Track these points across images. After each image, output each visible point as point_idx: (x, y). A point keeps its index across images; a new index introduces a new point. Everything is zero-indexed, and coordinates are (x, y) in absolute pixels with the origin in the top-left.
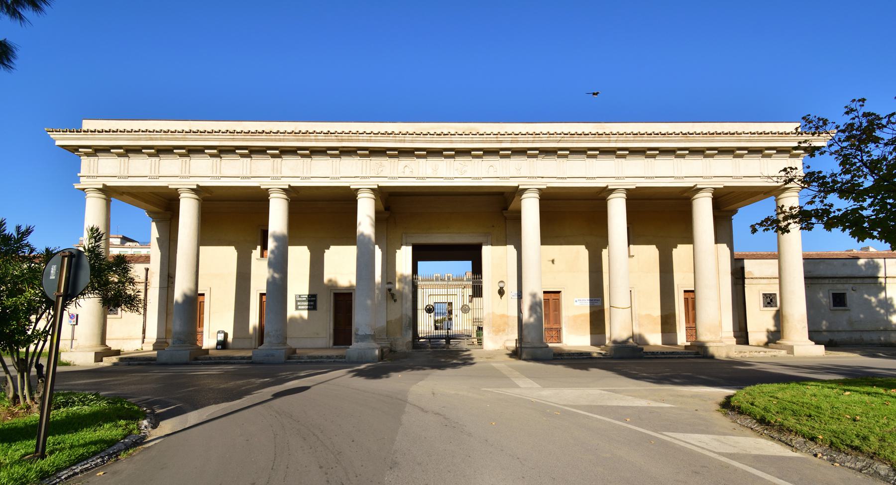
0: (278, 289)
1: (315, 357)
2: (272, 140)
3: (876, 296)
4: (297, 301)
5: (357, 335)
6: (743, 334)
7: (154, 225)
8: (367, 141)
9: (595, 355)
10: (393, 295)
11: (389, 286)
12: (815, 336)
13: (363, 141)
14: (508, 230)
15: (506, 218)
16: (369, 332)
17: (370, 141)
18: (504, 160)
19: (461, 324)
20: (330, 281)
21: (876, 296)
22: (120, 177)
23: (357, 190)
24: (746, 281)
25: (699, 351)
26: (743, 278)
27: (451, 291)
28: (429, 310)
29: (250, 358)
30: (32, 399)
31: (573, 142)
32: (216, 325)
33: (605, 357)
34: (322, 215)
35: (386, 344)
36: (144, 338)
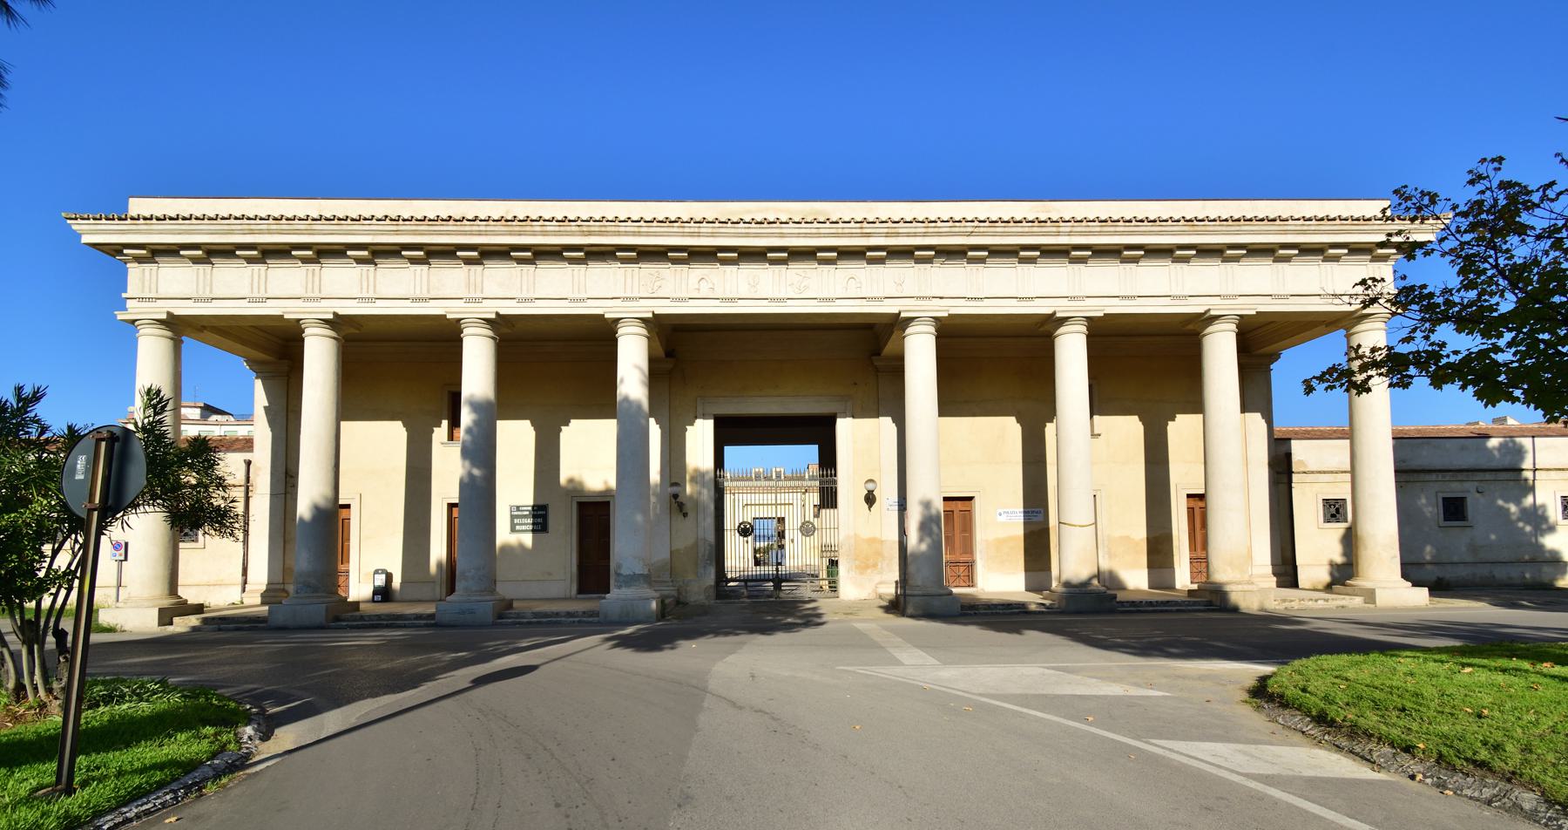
0: (479, 494)
1: (546, 615)
2: (464, 233)
3: (1518, 502)
4: (513, 517)
5: (618, 575)
6: (1289, 568)
7: (259, 384)
8: (634, 234)
9: (1033, 607)
10: (681, 506)
11: (675, 489)
12: (1412, 571)
13: (626, 234)
14: (884, 394)
15: (877, 370)
16: (639, 569)
17: (639, 234)
18: (874, 268)
19: (799, 555)
20: (571, 481)
21: (1518, 502)
22: (197, 300)
23: (617, 320)
24: (1295, 477)
25: (1212, 599)
26: (1289, 472)
27: (782, 498)
28: (745, 531)
29: (431, 616)
30: (49, 691)
31: (994, 235)
32: (372, 559)
33: (1049, 611)
34: (556, 365)
35: (669, 590)
36: (245, 582)
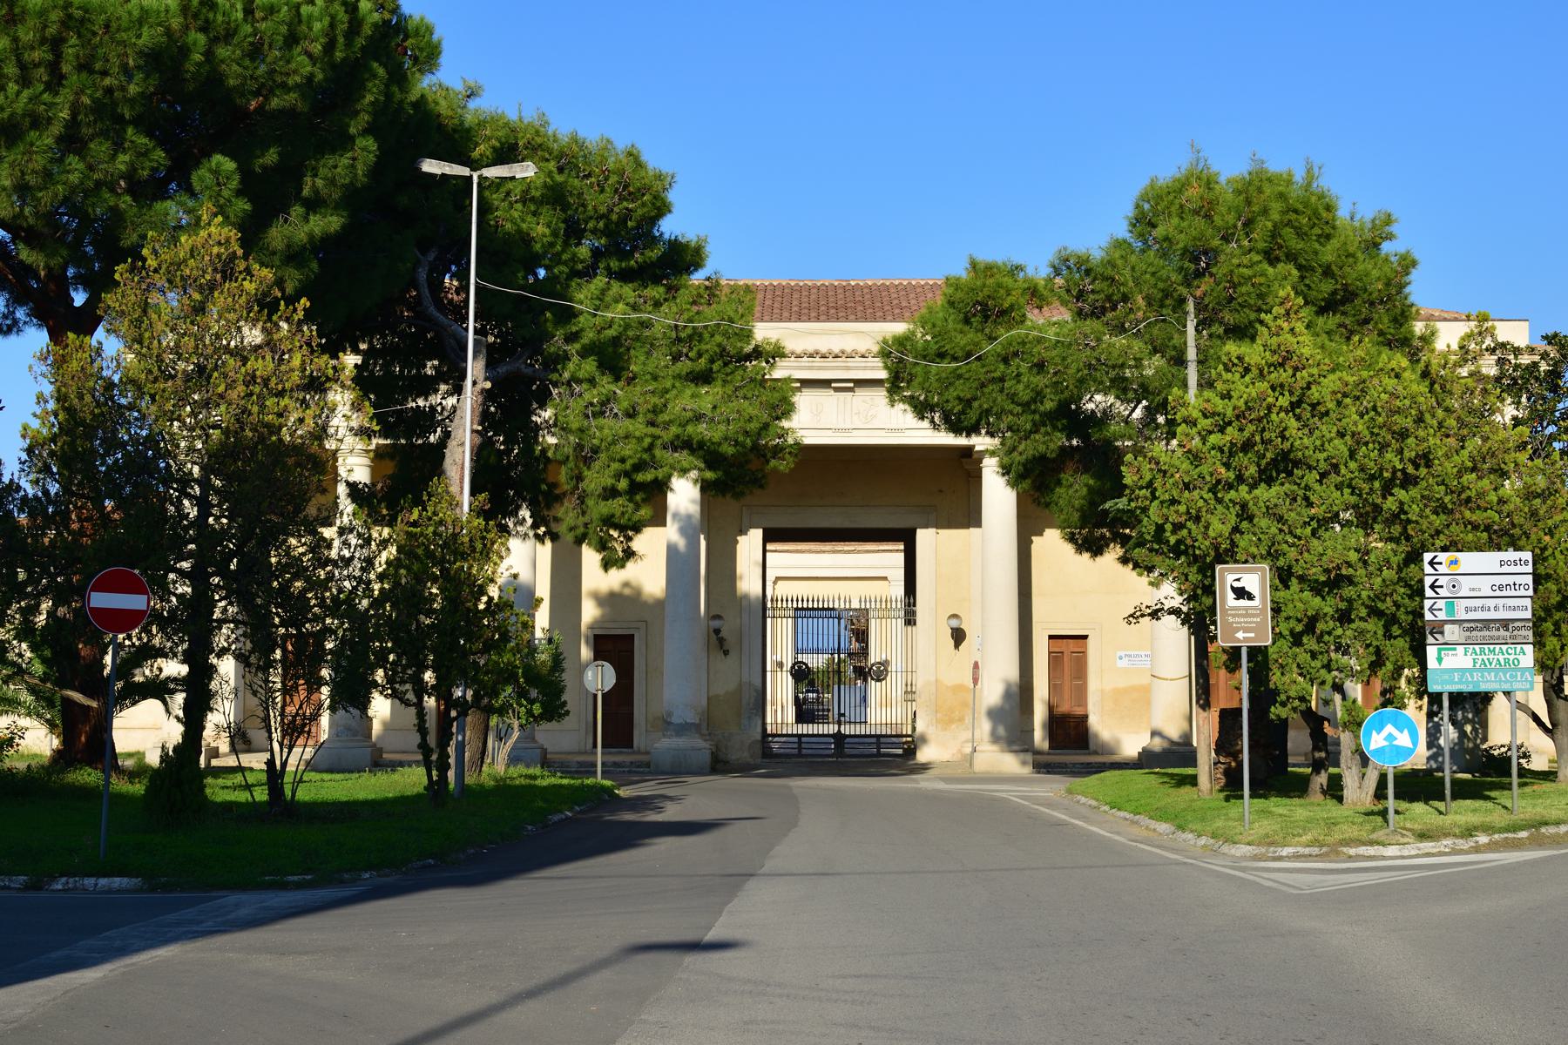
10: (721, 641)
11: (716, 624)
16: (691, 717)
